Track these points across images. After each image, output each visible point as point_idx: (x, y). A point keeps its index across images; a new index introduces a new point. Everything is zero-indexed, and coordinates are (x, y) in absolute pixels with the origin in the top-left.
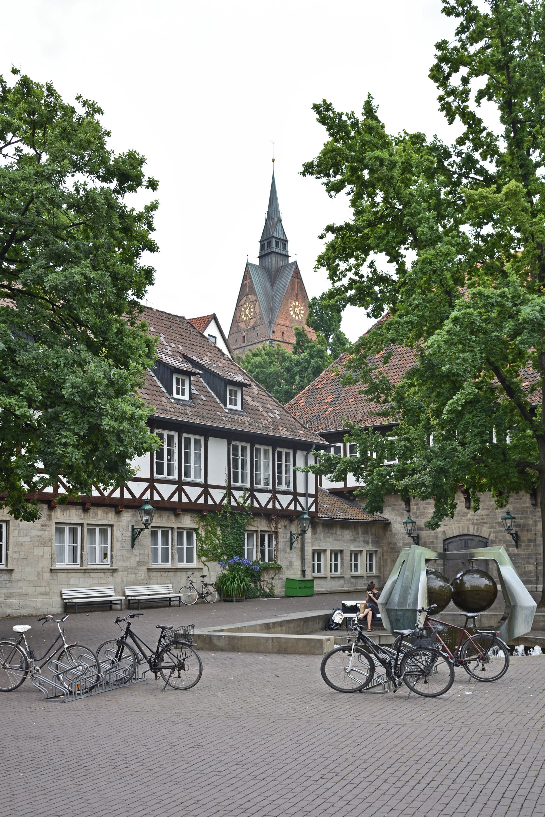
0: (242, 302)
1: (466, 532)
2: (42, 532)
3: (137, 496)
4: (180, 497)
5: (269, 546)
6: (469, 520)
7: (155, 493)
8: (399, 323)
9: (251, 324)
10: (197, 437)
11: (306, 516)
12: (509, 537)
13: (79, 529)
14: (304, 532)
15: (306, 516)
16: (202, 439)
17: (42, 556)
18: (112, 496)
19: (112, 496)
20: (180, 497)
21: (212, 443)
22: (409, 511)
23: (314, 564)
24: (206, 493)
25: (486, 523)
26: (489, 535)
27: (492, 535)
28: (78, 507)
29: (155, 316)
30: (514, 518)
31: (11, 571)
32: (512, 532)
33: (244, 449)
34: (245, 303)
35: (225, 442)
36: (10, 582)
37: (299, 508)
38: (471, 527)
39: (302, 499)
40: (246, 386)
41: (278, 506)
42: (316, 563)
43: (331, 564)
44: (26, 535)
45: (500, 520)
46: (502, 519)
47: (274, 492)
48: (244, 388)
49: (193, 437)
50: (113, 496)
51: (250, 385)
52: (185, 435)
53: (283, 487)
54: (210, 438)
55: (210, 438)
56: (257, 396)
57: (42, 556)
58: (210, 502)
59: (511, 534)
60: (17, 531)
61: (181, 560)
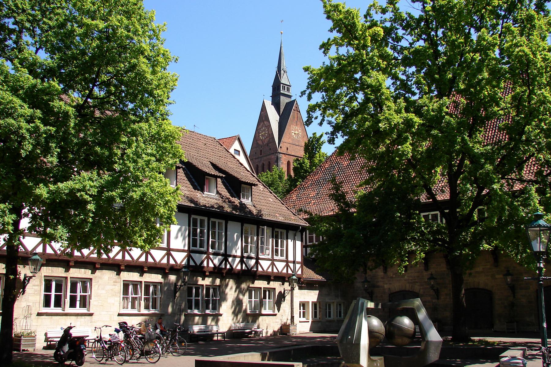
0: (260, 126)
1: (403, 289)
2: (114, 287)
3: (135, 258)
4: (168, 260)
5: (269, 299)
6: (405, 280)
7: (210, 261)
8: (534, 204)
9: (266, 142)
10: (220, 221)
11: (294, 277)
12: (432, 292)
13: (201, 288)
14: (292, 289)
15: (294, 277)
16: (224, 222)
17: (113, 304)
18: (116, 258)
19: (116, 258)
20: (168, 260)
21: (231, 224)
22: (366, 273)
23: (300, 312)
24: (169, 254)
25: (417, 282)
26: (420, 291)
27: (421, 290)
28: (139, 269)
29: (195, 137)
30: (436, 279)
31: (91, 315)
32: (435, 288)
33: (202, 222)
34: (262, 127)
35: (187, 215)
36: (91, 322)
37: (290, 272)
38: (408, 285)
39: (291, 265)
40: (255, 185)
41: (150, 260)
42: (328, 311)
43: (300, 312)
44: (103, 289)
45: (426, 280)
46: (428, 279)
47: (273, 260)
48: (253, 187)
49: (217, 221)
50: (162, 262)
51: (257, 185)
52: (212, 219)
53: (279, 257)
54: (229, 222)
55: (229, 222)
56: (262, 192)
57: (113, 304)
58: (275, 270)
59: (434, 290)
60: (97, 286)
61: (208, 308)
